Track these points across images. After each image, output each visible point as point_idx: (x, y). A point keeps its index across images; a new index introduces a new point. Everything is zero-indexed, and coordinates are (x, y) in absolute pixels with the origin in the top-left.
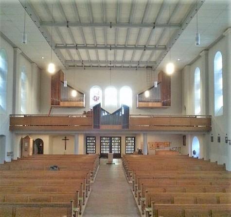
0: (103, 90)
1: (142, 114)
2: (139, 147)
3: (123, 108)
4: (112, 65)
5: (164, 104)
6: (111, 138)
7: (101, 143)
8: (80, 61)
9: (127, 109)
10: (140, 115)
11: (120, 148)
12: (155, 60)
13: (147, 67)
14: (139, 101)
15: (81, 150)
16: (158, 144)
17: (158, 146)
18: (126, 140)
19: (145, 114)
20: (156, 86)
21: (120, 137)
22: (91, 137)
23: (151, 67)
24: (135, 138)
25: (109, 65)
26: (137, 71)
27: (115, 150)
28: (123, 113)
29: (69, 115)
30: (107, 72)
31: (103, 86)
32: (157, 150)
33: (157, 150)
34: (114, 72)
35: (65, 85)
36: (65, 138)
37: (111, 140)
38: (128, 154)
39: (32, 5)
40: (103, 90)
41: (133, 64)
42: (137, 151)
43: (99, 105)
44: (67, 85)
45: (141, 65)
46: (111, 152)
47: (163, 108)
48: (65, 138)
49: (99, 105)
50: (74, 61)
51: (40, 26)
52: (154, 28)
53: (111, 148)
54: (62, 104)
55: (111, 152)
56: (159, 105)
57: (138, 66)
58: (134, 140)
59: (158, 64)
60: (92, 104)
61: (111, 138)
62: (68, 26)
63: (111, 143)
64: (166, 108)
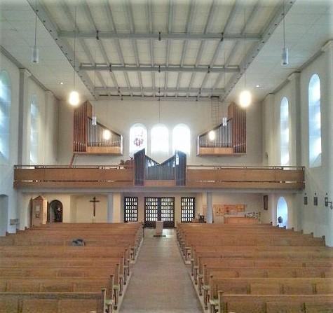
0: (148, 129)
1: (204, 165)
2: (200, 212)
3: (177, 156)
4: (161, 94)
5: (236, 150)
6: (160, 199)
7: (145, 206)
8: (115, 88)
9: (183, 158)
10: (202, 166)
11: (174, 213)
12: (223, 87)
13: (212, 97)
14: (201, 146)
15: (117, 217)
16: (227, 208)
17: (228, 211)
18: (182, 202)
19: (208, 165)
20: (225, 124)
21: (174, 198)
22: (131, 198)
23: (218, 97)
24: (194, 199)
25: (158, 94)
26: (198, 102)
27: (166, 216)
28: (177, 163)
29: (99, 166)
30: (155, 104)
31: (148, 124)
32: (227, 216)
33: (227, 216)
34: (164, 103)
35: (94, 123)
36: (94, 199)
37: (160, 202)
38: (184, 222)
39: (46, 7)
40: (148, 129)
41: (192, 92)
42: (197, 217)
43: (143, 151)
44: (97, 123)
45: (203, 94)
46: (160, 219)
47: (235, 155)
48: (94, 199)
49: (143, 151)
50: (107, 88)
51: (57, 38)
52: (222, 40)
53: (159, 213)
54: (89, 150)
55: (160, 219)
56: (229, 151)
57: (199, 95)
58: (194, 202)
59: (227, 92)
60: (133, 149)
61: (160, 199)
62: (98, 38)
63: (160, 206)
64: (240, 156)
